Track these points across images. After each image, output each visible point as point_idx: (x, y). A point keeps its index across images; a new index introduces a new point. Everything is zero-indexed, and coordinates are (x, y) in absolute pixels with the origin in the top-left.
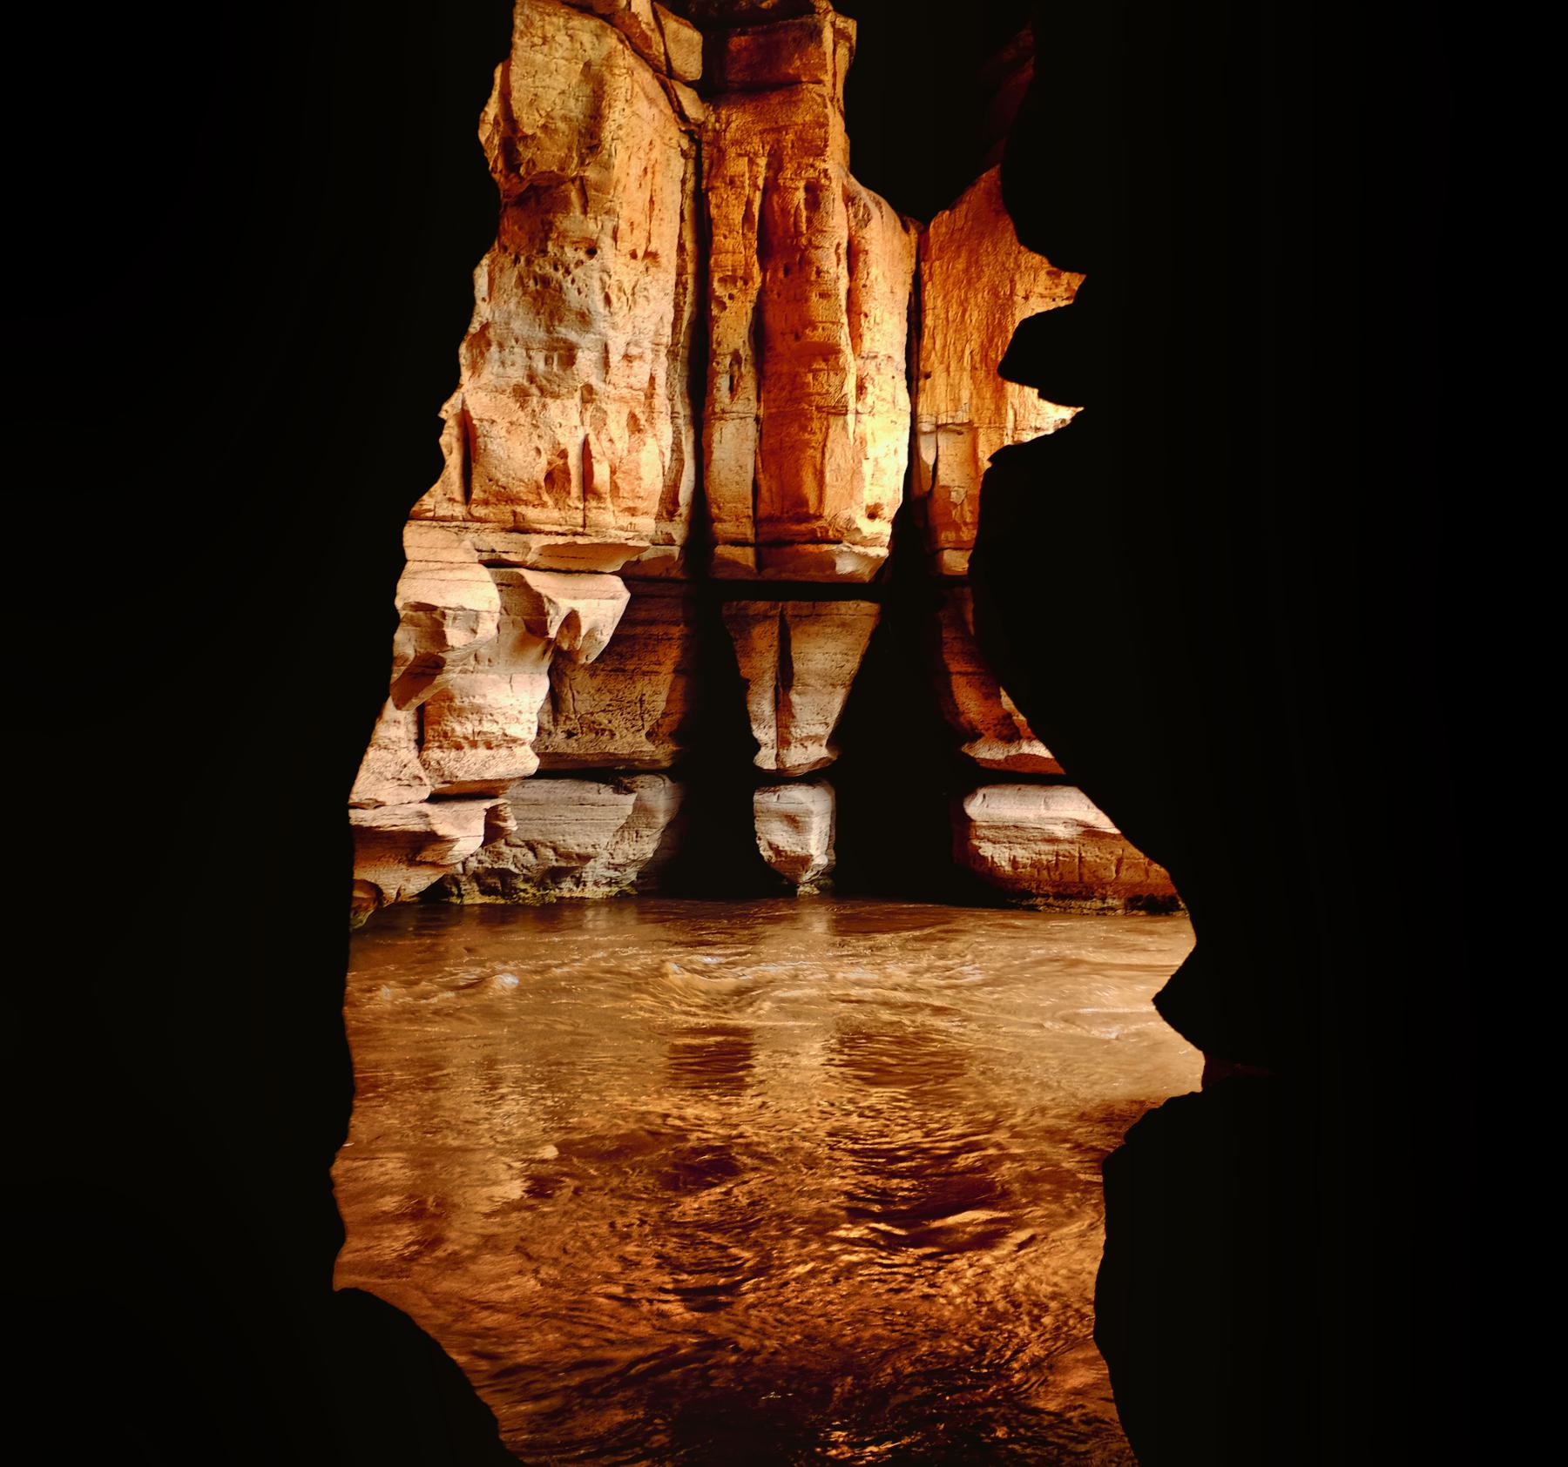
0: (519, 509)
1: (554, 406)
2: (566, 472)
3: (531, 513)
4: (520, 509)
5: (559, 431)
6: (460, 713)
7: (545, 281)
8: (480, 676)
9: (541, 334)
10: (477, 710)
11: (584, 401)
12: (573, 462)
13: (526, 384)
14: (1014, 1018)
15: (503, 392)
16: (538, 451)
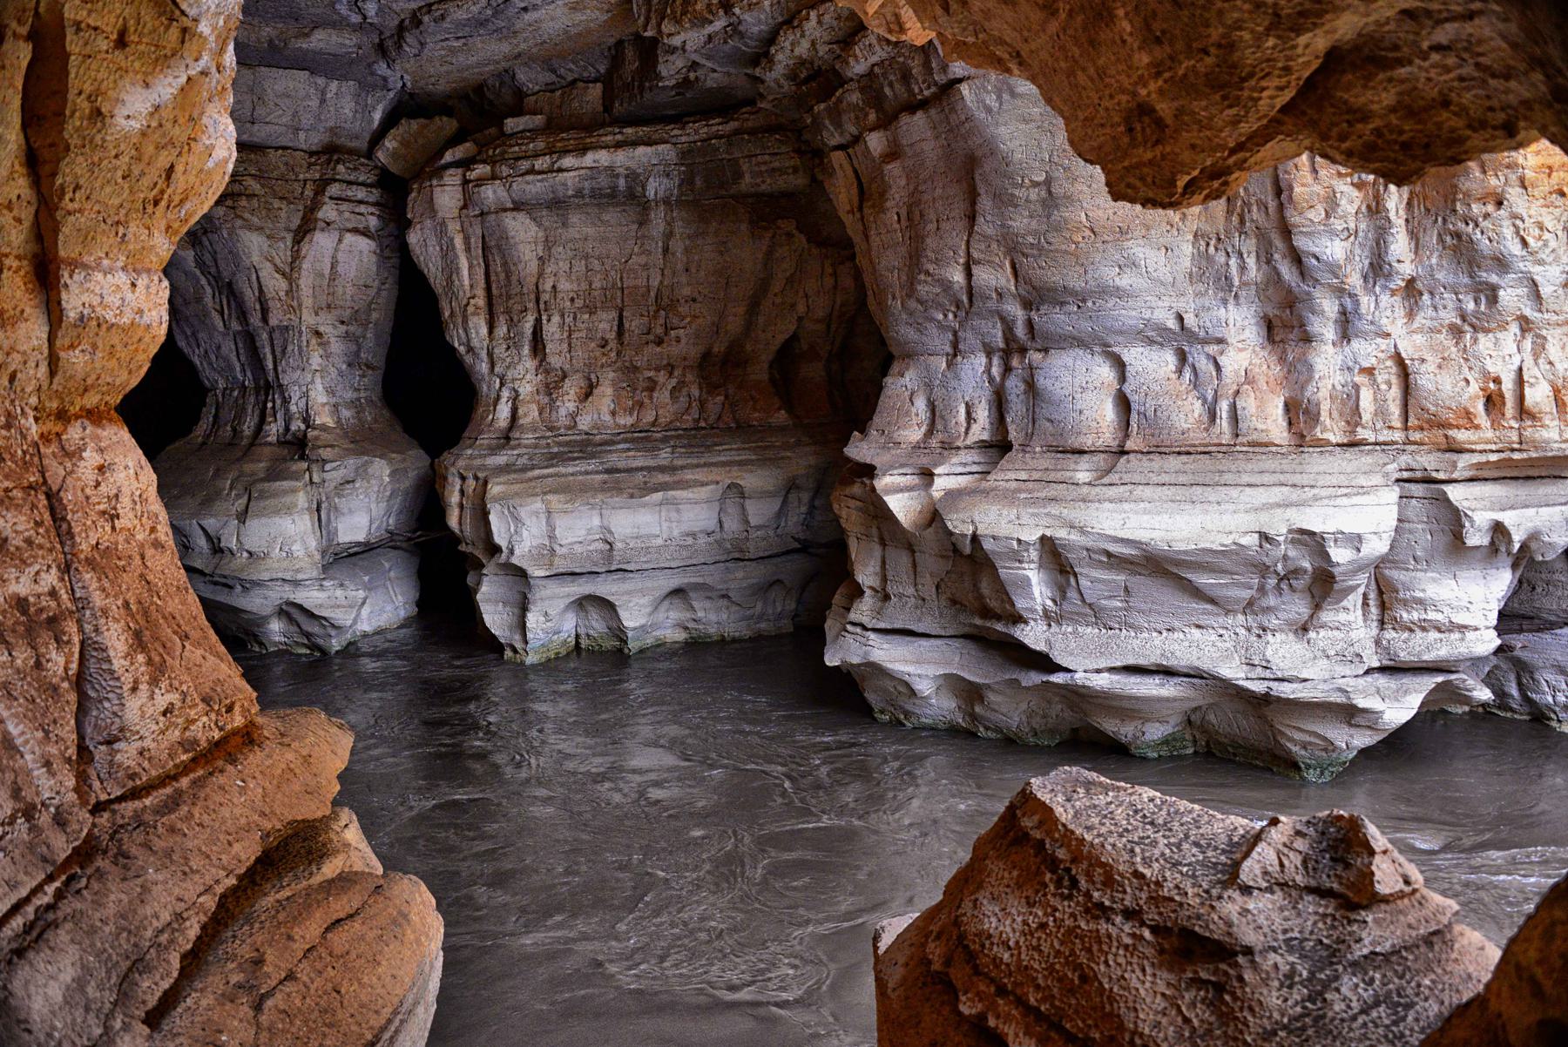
0: (1450, 433)
1: (1485, 342)
2: (1502, 396)
3: (1461, 436)
4: (1450, 433)
5: (1488, 362)
6: (1405, 603)
7: (1457, 235)
8: (1419, 574)
9: (1466, 280)
10: (1420, 602)
11: (1523, 330)
12: (1508, 386)
13: (1459, 322)
14: (559, 934)
15: (1439, 332)
16: (1467, 381)
